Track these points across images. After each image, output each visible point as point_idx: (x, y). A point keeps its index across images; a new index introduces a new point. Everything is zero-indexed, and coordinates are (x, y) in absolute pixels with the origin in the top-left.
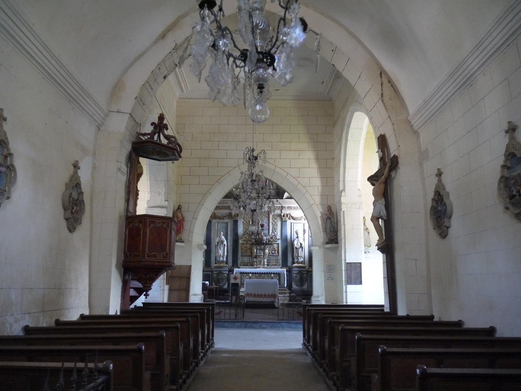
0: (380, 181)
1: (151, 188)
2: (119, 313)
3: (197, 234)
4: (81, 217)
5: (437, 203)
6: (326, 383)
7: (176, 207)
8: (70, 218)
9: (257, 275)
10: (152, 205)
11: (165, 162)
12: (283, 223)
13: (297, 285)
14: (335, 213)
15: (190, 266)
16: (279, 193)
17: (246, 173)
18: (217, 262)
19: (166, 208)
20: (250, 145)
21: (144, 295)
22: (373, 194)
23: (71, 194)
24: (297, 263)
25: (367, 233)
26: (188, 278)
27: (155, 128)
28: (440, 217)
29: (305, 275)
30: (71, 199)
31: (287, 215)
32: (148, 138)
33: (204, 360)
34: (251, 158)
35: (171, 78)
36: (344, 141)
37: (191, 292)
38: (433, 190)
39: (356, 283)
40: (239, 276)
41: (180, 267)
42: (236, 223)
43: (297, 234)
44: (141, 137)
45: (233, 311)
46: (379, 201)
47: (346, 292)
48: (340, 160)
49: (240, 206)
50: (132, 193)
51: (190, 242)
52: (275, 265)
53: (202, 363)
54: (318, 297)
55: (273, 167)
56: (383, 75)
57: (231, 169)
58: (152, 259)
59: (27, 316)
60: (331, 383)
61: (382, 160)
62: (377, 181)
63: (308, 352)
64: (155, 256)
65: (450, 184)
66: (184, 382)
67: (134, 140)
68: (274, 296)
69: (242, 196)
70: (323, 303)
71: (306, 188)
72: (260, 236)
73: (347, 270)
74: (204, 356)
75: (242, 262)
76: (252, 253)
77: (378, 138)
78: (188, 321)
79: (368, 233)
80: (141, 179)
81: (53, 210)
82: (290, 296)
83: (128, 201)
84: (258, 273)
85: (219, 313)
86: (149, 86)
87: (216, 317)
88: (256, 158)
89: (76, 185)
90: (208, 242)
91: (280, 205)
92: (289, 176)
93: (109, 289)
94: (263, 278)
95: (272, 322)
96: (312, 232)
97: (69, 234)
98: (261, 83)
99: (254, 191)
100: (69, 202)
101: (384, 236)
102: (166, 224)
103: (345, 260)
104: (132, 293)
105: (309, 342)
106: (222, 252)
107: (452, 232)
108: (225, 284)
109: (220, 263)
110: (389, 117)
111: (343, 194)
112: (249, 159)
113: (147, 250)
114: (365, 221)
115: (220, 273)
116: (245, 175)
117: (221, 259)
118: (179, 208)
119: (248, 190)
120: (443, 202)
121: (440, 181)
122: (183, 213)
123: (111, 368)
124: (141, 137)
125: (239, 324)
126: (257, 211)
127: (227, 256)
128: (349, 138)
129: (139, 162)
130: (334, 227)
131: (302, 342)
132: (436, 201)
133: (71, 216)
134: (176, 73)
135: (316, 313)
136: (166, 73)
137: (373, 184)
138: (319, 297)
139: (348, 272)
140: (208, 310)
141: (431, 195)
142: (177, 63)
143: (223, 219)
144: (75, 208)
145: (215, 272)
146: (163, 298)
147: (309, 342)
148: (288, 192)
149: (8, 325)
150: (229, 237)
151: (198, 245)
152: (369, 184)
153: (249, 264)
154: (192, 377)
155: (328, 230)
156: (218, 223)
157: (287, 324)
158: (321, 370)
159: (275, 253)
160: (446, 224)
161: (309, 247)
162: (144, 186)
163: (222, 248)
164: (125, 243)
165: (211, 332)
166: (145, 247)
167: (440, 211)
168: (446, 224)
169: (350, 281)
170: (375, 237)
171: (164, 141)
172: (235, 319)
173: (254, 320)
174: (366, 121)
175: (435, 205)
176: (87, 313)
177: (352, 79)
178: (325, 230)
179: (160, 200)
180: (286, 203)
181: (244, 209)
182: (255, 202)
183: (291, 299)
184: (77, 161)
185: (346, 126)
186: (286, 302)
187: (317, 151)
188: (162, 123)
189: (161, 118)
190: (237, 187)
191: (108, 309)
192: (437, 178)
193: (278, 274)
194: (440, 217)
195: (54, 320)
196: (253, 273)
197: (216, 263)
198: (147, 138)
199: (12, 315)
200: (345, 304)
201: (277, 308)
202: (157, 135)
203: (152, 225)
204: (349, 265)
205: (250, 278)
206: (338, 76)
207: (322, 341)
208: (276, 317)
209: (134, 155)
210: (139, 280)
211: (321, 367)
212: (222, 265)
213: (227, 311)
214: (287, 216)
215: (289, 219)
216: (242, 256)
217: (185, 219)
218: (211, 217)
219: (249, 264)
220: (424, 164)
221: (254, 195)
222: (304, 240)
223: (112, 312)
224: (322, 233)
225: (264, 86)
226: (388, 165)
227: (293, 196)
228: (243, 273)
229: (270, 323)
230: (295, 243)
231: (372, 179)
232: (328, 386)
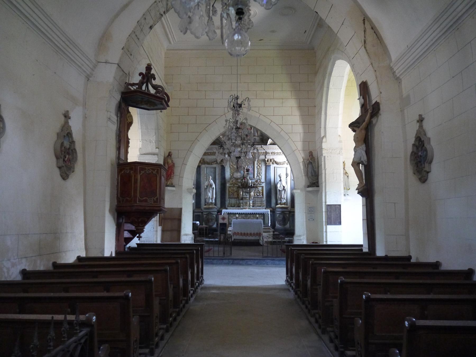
0: (361, 127)
1: (142, 136)
2: (114, 255)
3: (187, 178)
4: (74, 166)
5: (417, 148)
6: (308, 319)
7: (167, 154)
8: (63, 166)
9: (244, 215)
10: (144, 152)
11: (155, 111)
12: (267, 167)
13: (280, 224)
14: (316, 158)
15: (181, 209)
16: (264, 140)
17: (231, 120)
18: (206, 203)
19: (157, 155)
20: (234, 93)
21: (137, 237)
22: (354, 140)
23: (62, 144)
24: (281, 204)
25: (346, 177)
26: (179, 220)
27: (143, 78)
28: (420, 162)
29: (288, 215)
30: (63, 148)
31: (271, 160)
32: (137, 88)
33: (194, 296)
34: (235, 105)
35: (158, 27)
36: (325, 89)
37: (183, 232)
38: (414, 135)
39: (335, 224)
40: (226, 216)
41: (172, 209)
42: (223, 169)
43: (280, 178)
44: (130, 87)
45: (221, 249)
46: (360, 147)
47: (326, 232)
48: (321, 108)
49: (225, 154)
50: (122, 141)
51: (181, 186)
52: (260, 206)
53: (192, 299)
54: (300, 236)
55: (257, 115)
56: (366, 22)
57: (219, 116)
58: (144, 204)
59: (24, 260)
60: (313, 320)
61: (363, 107)
62: (359, 127)
63: (291, 289)
64: (146, 201)
65: (430, 128)
66: (175, 319)
67: (123, 90)
68: (260, 235)
69: (227, 143)
70: (305, 243)
71: (289, 135)
72: (246, 180)
73: (327, 211)
74: (194, 293)
75: (229, 204)
76: (238, 195)
77: (360, 85)
78: (177, 263)
79: (348, 176)
80: (131, 128)
81: (43, 159)
82: (274, 235)
83: (119, 149)
84: (244, 214)
85: (209, 251)
86: (136, 36)
87: (206, 254)
88: (240, 106)
89: (67, 135)
90: (198, 186)
91: (264, 151)
92: (272, 124)
93: (104, 232)
94: (249, 218)
95: (257, 260)
96: (295, 176)
97: (63, 182)
98: (240, 7)
99: (239, 139)
100: (61, 151)
101: (364, 180)
102: (156, 171)
103: (326, 202)
104: (126, 235)
105: (291, 279)
106: (211, 195)
107: (432, 176)
108: (214, 224)
109: (210, 205)
110: (372, 64)
111: (324, 140)
112: (234, 106)
113: (138, 195)
114: (344, 165)
115: (210, 213)
116: (229, 122)
117: (210, 201)
118: (170, 155)
119: (233, 137)
120: (424, 148)
121: (421, 126)
122: (173, 159)
123: (94, 321)
124: (130, 87)
125: (227, 261)
126: (242, 158)
127: (216, 198)
128: (331, 86)
129: (129, 112)
130: (315, 171)
131: (285, 279)
132: (416, 146)
133: (64, 165)
134: (163, 24)
135: (298, 253)
136: (151, 23)
137: (354, 131)
138: (301, 237)
139: (328, 213)
140: (197, 250)
141: (412, 140)
142: (162, 13)
143: (212, 164)
144: (67, 156)
145: (205, 213)
146: (157, 238)
147: (292, 279)
148: (271, 139)
149: (5, 270)
150: (217, 181)
151: (187, 189)
152: (350, 130)
153: (236, 206)
154: (183, 313)
155: (310, 175)
156: (207, 168)
157: (272, 261)
158: (303, 306)
159: (260, 195)
160: (427, 169)
161: (292, 189)
162: (135, 135)
163: (211, 191)
164: (118, 190)
165: (200, 270)
166: (137, 191)
167: (421, 156)
168: (427, 169)
169: (330, 222)
170: (355, 181)
171: (152, 91)
172: (223, 257)
173: (240, 258)
174: (348, 68)
175: (415, 150)
176: (83, 255)
177: (335, 29)
178: (307, 175)
179: (152, 148)
180: (270, 148)
181: (229, 156)
182: (239, 149)
183: (275, 236)
184: (68, 111)
185: (327, 75)
186: (270, 240)
187: (299, 99)
188: (150, 73)
189: (149, 68)
190: (224, 135)
191: (103, 250)
192: (418, 124)
193: (263, 215)
194: (420, 162)
195: (51, 263)
196: (240, 214)
197: (205, 205)
198: (135, 88)
199: (9, 260)
200: (325, 243)
201: (261, 245)
202: (145, 85)
203: (142, 172)
204: (329, 207)
205: (237, 218)
206: (320, 24)
207: (305, 280)
208: (262, 255)
209: (123, 105)
210: (132, 223)
211: (304, 303)
212: (211, 206)
213: (216, 248)
214: (271, 161)
215: (273, 164)
216: (229, 198)
217: (175, 165)
218: (200, 161)
219: (236, 206)
220: (405, 111)
221: (239, 142)
222: (287, 183)
223: (107, 254)
224: (304, 177)
225: (244, 11)
226: (370, 111)
227: (276, 142)
228: (231, 213)
229: (255, 260)
230: (279, 186)
231: (353, 126)
232: (310, 323)
